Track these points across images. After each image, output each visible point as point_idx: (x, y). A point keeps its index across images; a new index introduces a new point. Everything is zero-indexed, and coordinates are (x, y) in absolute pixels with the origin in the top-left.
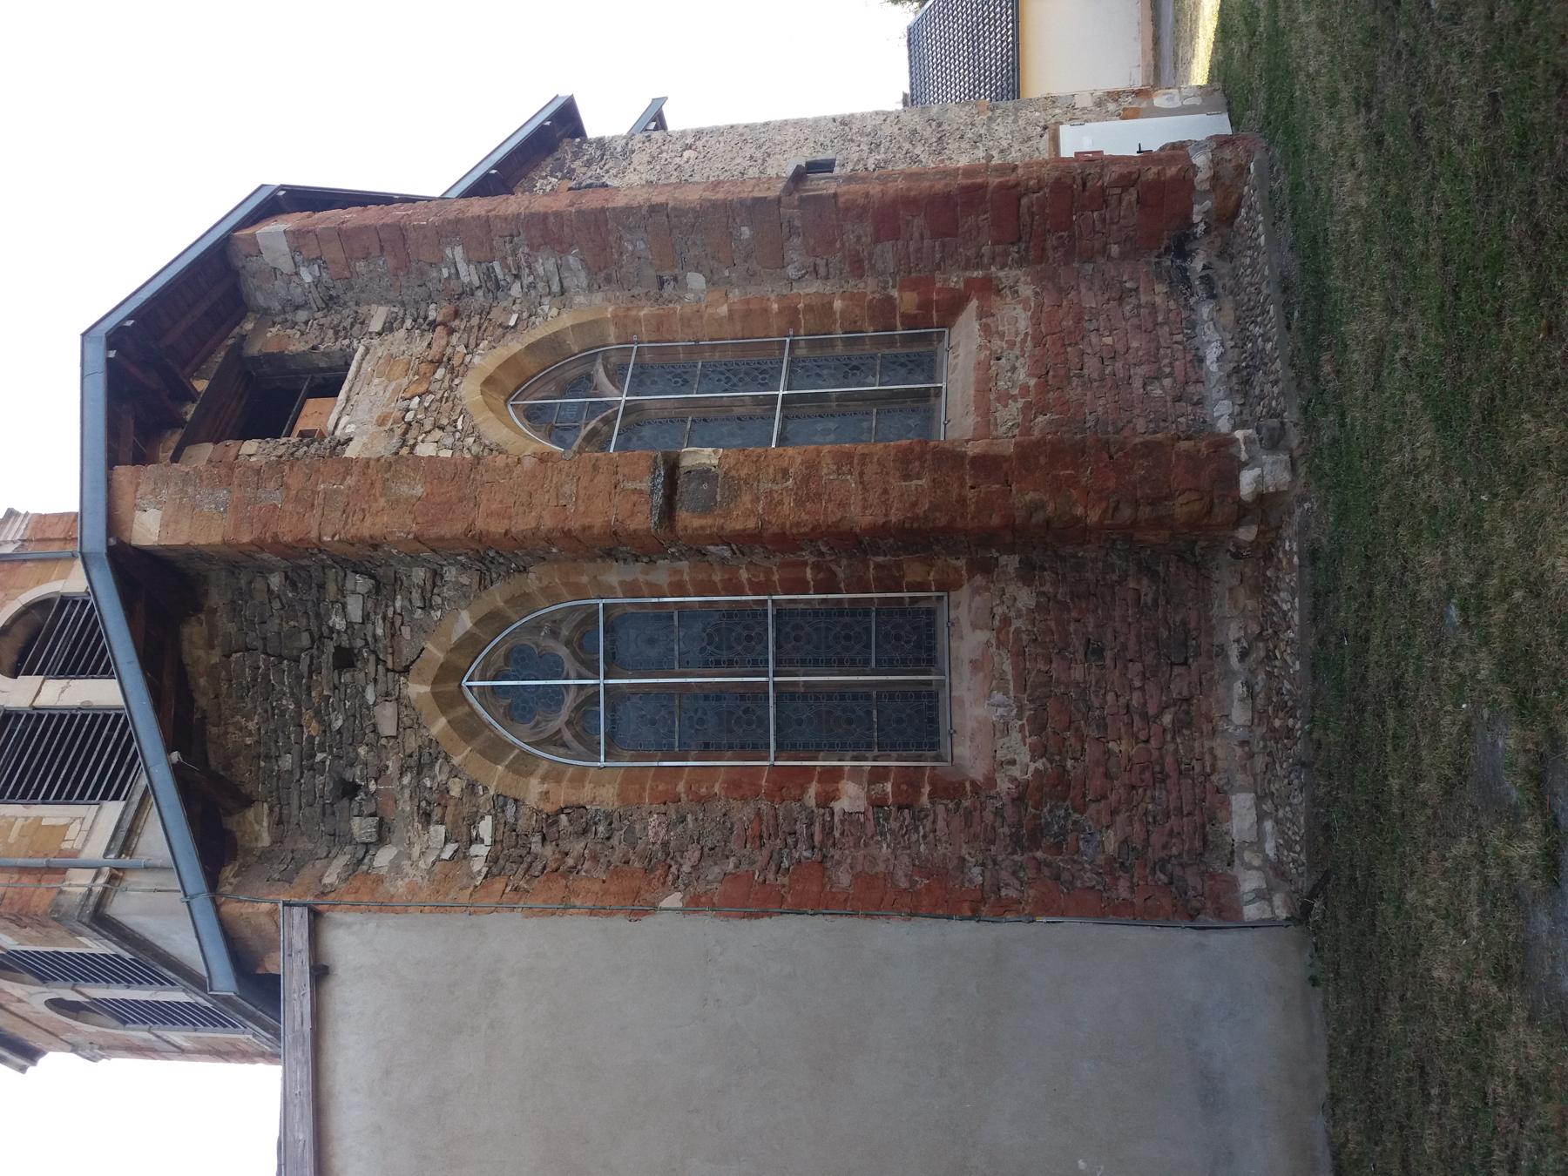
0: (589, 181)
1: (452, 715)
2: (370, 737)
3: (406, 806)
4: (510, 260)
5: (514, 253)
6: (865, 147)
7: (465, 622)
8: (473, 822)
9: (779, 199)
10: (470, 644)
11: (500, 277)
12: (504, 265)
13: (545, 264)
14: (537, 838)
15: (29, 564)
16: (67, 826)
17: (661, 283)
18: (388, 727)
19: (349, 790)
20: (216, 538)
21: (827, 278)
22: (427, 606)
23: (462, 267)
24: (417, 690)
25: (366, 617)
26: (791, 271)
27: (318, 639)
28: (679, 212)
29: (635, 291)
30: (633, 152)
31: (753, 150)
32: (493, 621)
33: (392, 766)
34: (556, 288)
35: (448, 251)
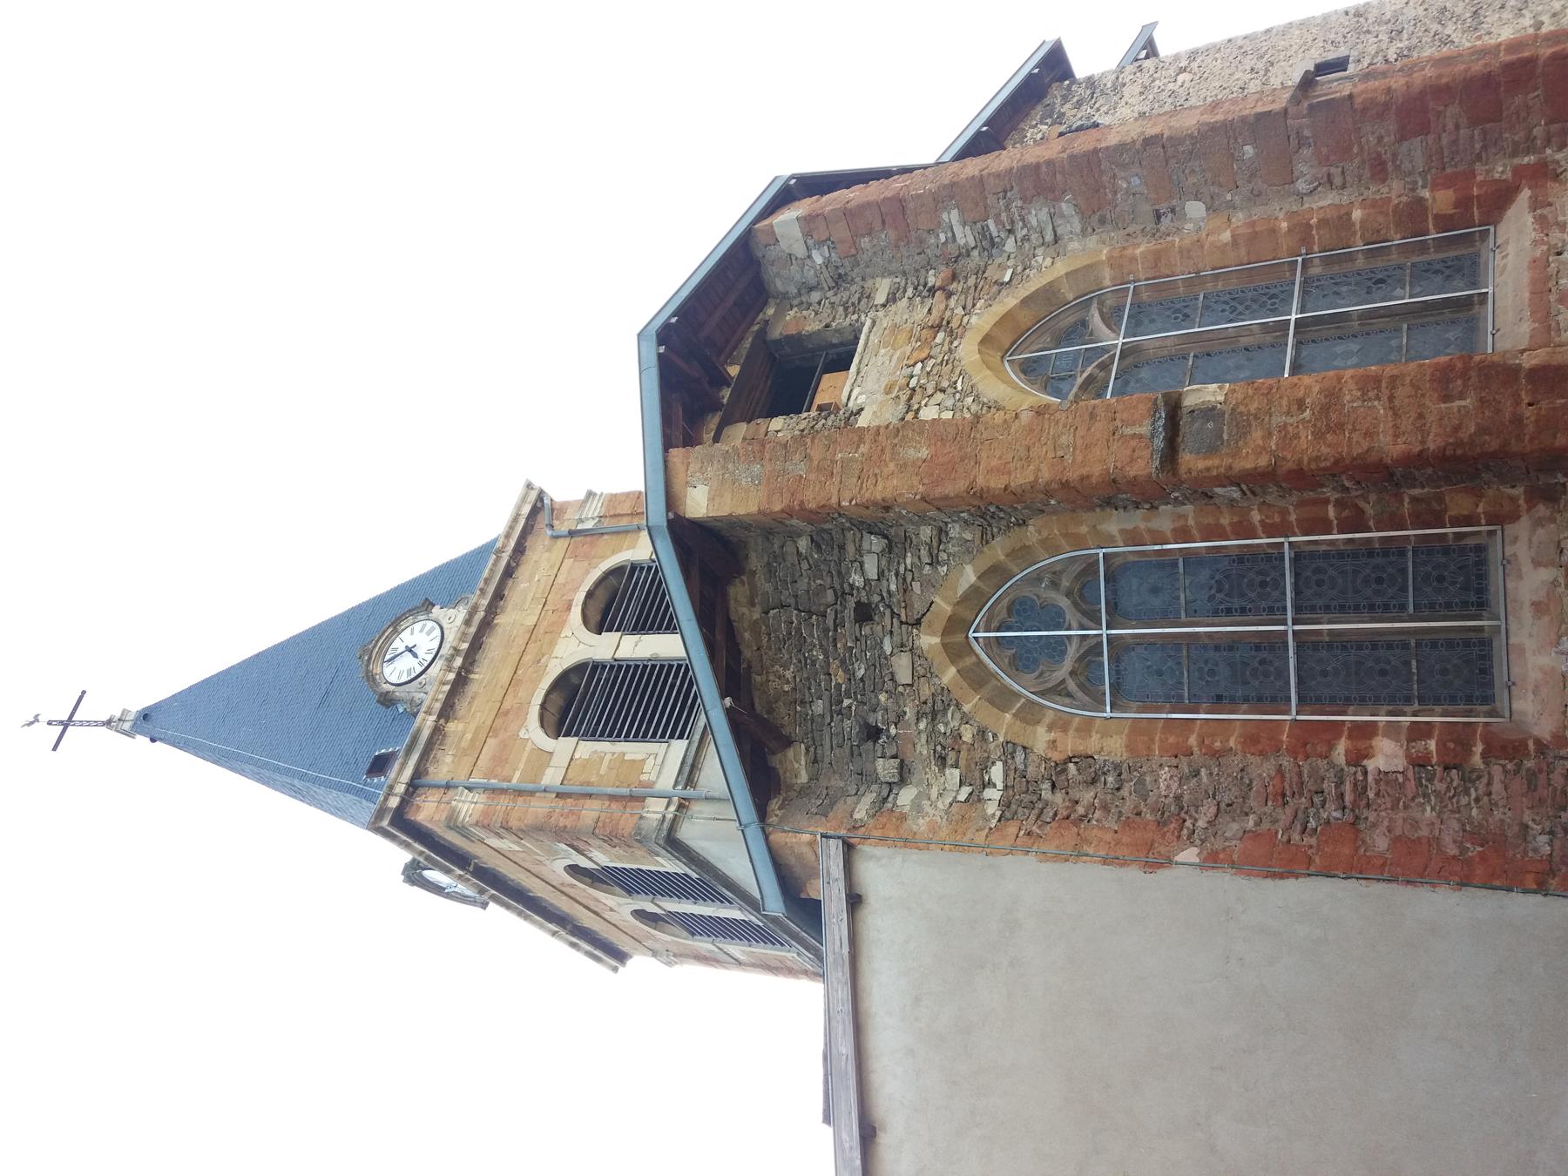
0: (1079, 123)
2: (889, 685)
3: (923, 749)
4: (1004, 216)
5: (1008, 208)
6: (1384, 37)
7: (969, 576)
8: (985, 767)
9: (1286, 110)
10: (974, 597)
11: (995, 234)
12: (998, 222)
13: (1038, 215)
14: (1046, 785)
15: (606, 537)
16: (644, 761)
17: (1158, 216)
18: (904, 676)
21: (1344, 187)
22: (934, 562)
23: (958, 230)
24: (928, 641)
25: (881, 574)
26: (1301, 186)
27: (841, 595)
28: (1176, 141)
29: (1130, 230)
30: (1124, 85)
31: (1255, 61)
32: (995, 574)
34: (1049, 237)
35: (945, 216)
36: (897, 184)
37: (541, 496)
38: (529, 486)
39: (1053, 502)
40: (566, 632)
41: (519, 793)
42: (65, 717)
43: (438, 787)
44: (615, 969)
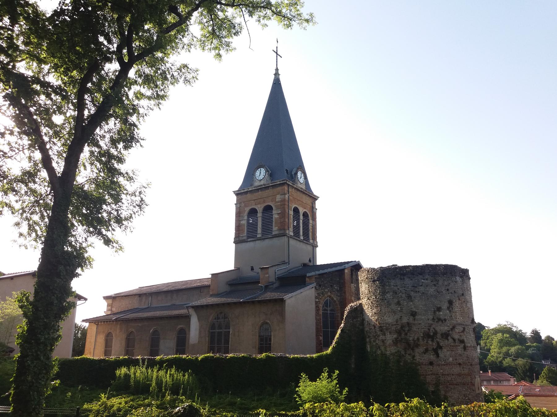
1: (358, 303)
3: (319, 292)
7: (335, 299)
10: (333, 299)
18: (326, 290)
19: (320, 286)
20: (346, 278)
22: (336, 295)
24: (329, 294)
32: (335, 301)
33: (322, 291)
36: (353, 263)
37: (317, 199)
38: (319, 197)
39: (45, 389)
40: (303, 209)
41: (288, 205)
42: (278, 53)
43: (288, 189)
44: (234, 192)
